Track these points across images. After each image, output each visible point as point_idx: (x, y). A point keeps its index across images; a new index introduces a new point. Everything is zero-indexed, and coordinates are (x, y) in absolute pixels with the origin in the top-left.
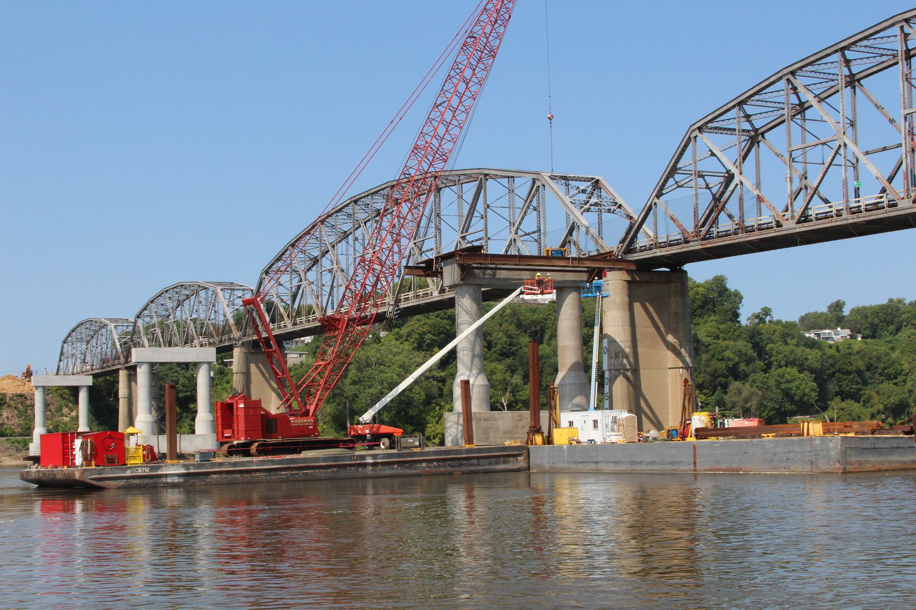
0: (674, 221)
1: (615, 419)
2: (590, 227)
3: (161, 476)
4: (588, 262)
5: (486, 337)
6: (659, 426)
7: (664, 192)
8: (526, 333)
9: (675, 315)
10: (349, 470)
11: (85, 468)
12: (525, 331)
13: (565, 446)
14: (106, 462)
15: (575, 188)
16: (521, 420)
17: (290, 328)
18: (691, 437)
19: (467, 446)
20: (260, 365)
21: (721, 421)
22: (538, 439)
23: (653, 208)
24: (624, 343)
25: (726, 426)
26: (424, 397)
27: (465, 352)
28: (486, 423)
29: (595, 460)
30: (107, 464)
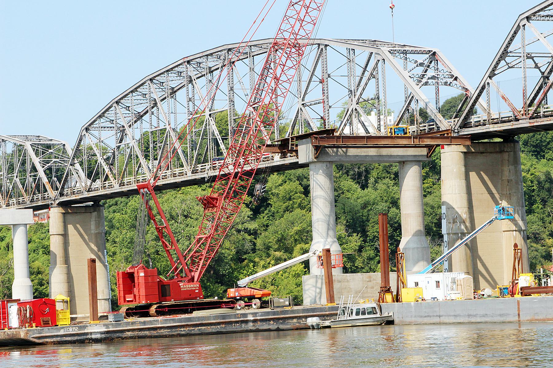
0: (506, 100)
1: (454, 280)
2: (429, 102)
3: (87, 334)
4: (428, 140)
5: (302, 180)
6: (493, 284)
7: (496, 72)
8: (348, 175)
9: (508, 182)
10: (235, 325)
11: (27, 329)
12: (347, 173)
13: (412, 303)
14: (42, 323)
15: (413, 61)
16: (370, 281)
17: (117, 189)
18: (518, 294)
19: (330, 305)
20: (78, 226)
21: (545, 280)
22: (388, 297)
23: (486, 87)
24: (462, 211)
25: (549, 285)
26: (234, 252)
27: (320, 223)
28: (340, 284)
29: (438, 314)
30: (43, 325)
